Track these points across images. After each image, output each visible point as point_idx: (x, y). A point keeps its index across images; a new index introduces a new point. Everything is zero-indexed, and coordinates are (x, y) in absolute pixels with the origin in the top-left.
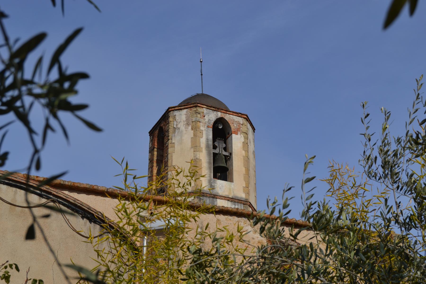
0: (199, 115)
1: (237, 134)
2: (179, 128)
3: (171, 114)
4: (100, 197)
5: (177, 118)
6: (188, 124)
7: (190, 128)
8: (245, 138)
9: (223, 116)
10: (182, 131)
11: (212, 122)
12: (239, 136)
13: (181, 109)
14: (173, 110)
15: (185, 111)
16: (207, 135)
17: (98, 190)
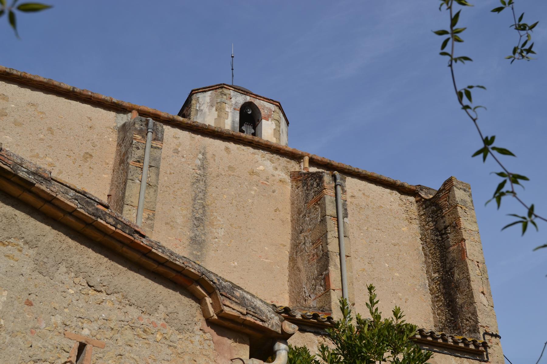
0: (225, 97)
1: (268, 120)
2: (202, 110)
3: (194, 97)
4: (63, 99)
5: (200, 100)
6: (212, 106)
7: (214, 109)
8: (276, 125)
9: (252, 101)
10: (205, 113)
11: (240, 106)
12: (269, 122)
13: (205, 91)
14: (197, 93)
15: (210, 92)
16: (233, 117)
17: (60, 88)
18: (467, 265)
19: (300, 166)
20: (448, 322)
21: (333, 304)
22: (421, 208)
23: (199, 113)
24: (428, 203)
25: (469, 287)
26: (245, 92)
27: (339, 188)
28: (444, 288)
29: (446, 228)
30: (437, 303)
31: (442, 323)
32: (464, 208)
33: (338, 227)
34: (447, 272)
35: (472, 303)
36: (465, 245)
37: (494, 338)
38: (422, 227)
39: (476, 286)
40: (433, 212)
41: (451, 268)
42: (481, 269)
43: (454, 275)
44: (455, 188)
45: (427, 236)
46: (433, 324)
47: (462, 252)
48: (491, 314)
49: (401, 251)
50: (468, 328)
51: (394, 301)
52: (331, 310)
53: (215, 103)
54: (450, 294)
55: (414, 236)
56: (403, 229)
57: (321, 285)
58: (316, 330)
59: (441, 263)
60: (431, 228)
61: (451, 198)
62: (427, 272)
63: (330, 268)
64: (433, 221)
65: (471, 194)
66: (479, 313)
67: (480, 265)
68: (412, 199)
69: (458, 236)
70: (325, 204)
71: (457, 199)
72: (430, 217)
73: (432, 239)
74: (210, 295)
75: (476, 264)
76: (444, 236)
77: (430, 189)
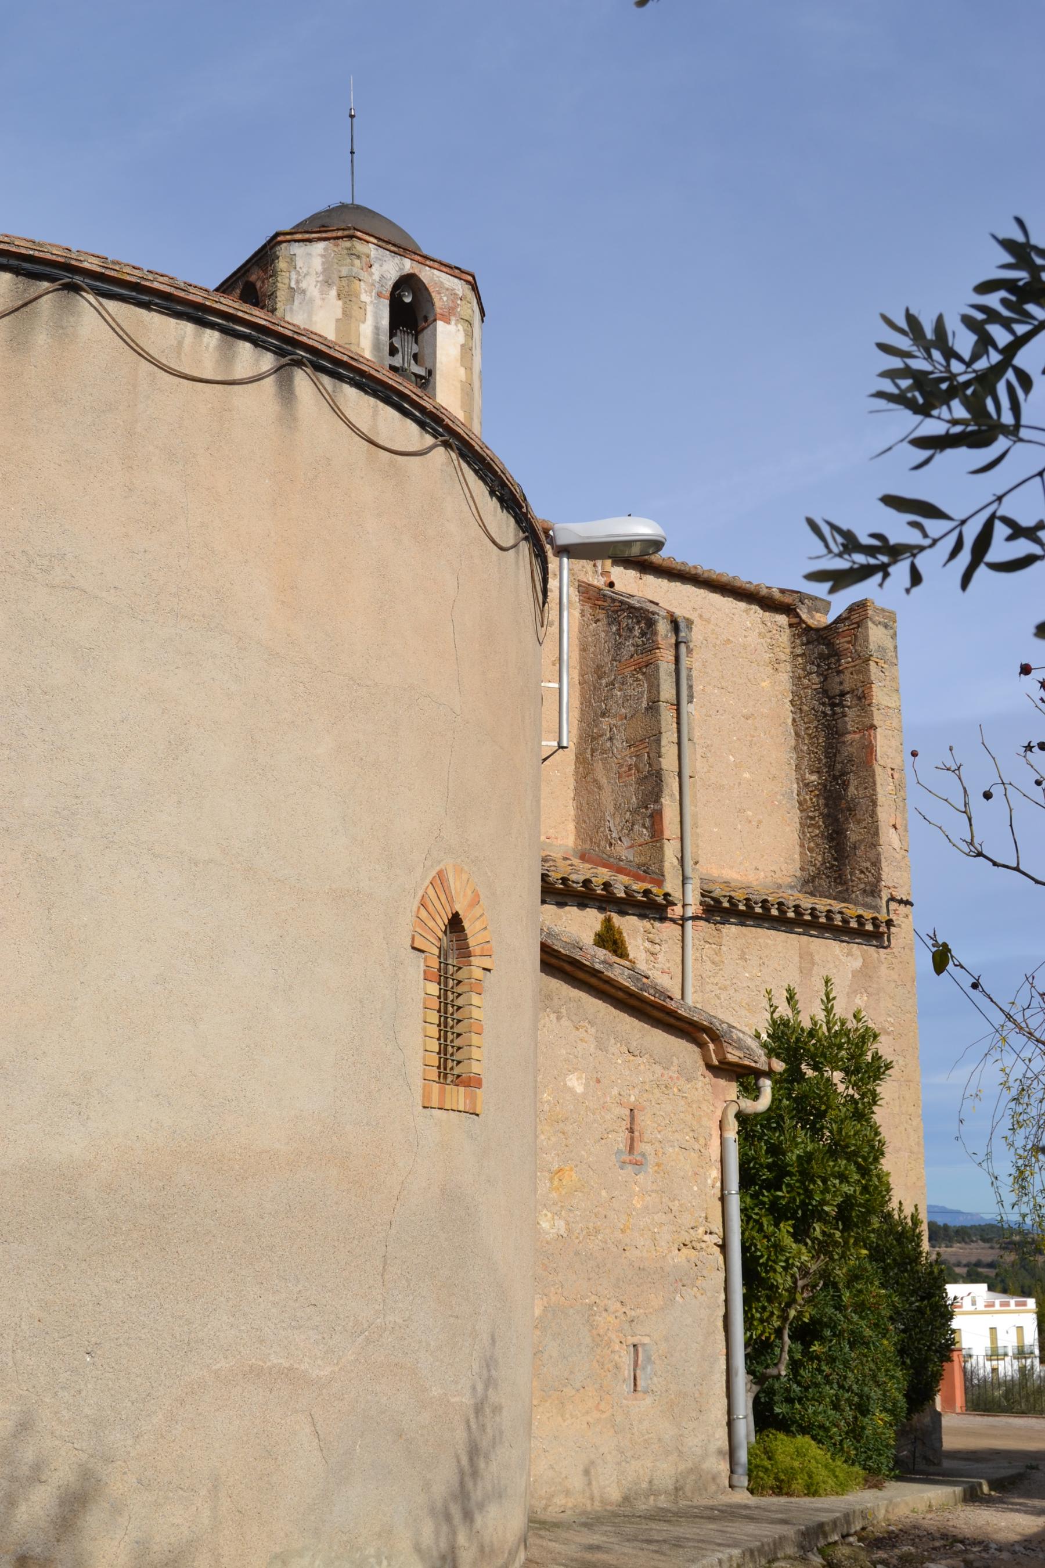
0: (357, 262)
1: (448, 322)
2: (304, 292)
7: (333, 293)
11: (390, 284)
16: (377, 317)
18: (873, 776)
19: (595, 565)
20: (826, 868)
21: (667, 865)
22: (798, 641)
23: (298, 298)
24: (812, 634)
25: (873, 814)
26: (402, 247)
27: (683, 648)
28: (826, 805)
29: (843, 694)
30: (810, 830)
31: (814, 866)
32: (881, 663)
33: (678, 723)
34: (835, 778)
35: (875, 845)
36: (875, 737)
37: (902, 906)
38: (796, 680)
39: (885, 815)
40: (821, 656)
41: (843, 774)
42: (897, 782)
43: (847, 788)
44: (870, 624)
45: (804, 700)
46: (798, 865)
47: (869, 749)
48: (902, 864)
49: (756, 729)
50: (862, 886)
51: (739, 826)
52: (663, 876)
53: (335, 277)
54: (837, 820)
55: (780, 696)
56: (763, 684)
57: (644, 826)
58: (642, 912)
59: (826, 757)
60: (814, 687)
61: (860, 641)
62: (798, 767)
63: (663, 800)
64: (819, 674)
65: (895, 634)
66: (884, 864)
67: (896, 776)
68: (782, 619)
69: (865, 717)
70: (658, 679)
71: (872, 647)
72: (813, 663)
73: (813, 709)
74: (712, 1040)
75: (890, 772)
76: (838, 709)
77: (816, 598)
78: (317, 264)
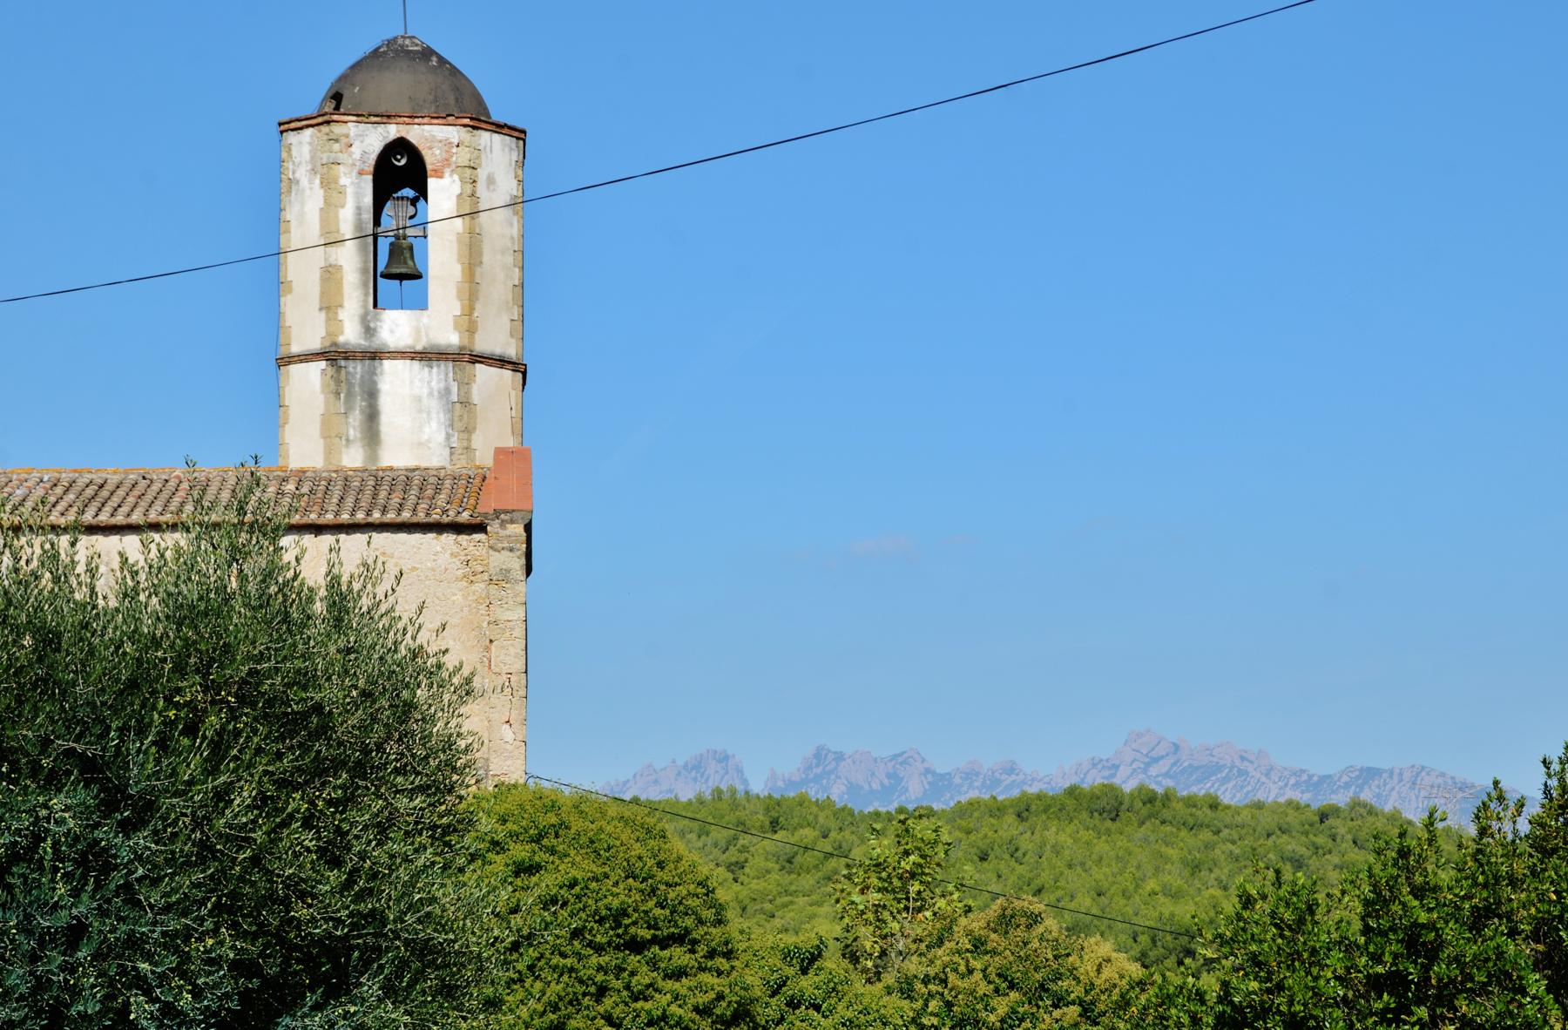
0: (336, 146)
7: (317, 181)
9: (403, 134)
16: (358, 196)
78: (306, 149)
